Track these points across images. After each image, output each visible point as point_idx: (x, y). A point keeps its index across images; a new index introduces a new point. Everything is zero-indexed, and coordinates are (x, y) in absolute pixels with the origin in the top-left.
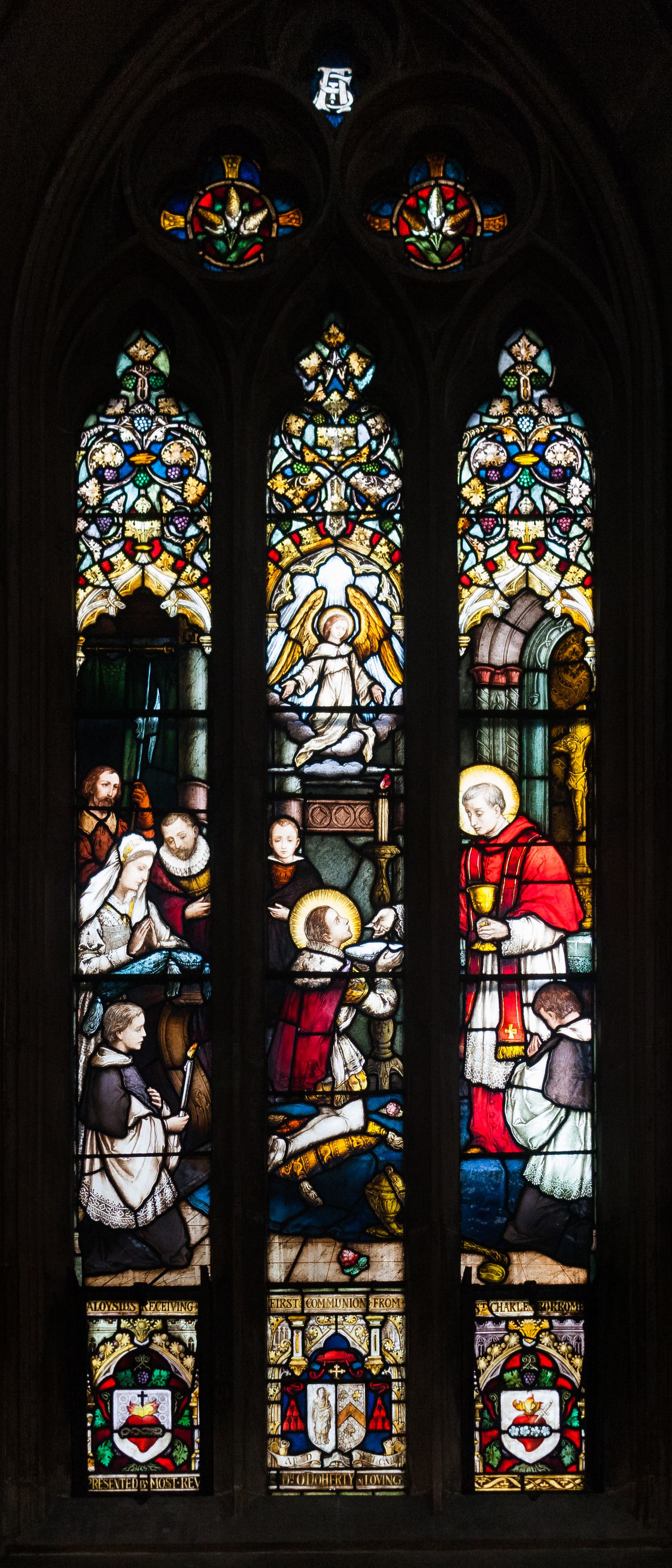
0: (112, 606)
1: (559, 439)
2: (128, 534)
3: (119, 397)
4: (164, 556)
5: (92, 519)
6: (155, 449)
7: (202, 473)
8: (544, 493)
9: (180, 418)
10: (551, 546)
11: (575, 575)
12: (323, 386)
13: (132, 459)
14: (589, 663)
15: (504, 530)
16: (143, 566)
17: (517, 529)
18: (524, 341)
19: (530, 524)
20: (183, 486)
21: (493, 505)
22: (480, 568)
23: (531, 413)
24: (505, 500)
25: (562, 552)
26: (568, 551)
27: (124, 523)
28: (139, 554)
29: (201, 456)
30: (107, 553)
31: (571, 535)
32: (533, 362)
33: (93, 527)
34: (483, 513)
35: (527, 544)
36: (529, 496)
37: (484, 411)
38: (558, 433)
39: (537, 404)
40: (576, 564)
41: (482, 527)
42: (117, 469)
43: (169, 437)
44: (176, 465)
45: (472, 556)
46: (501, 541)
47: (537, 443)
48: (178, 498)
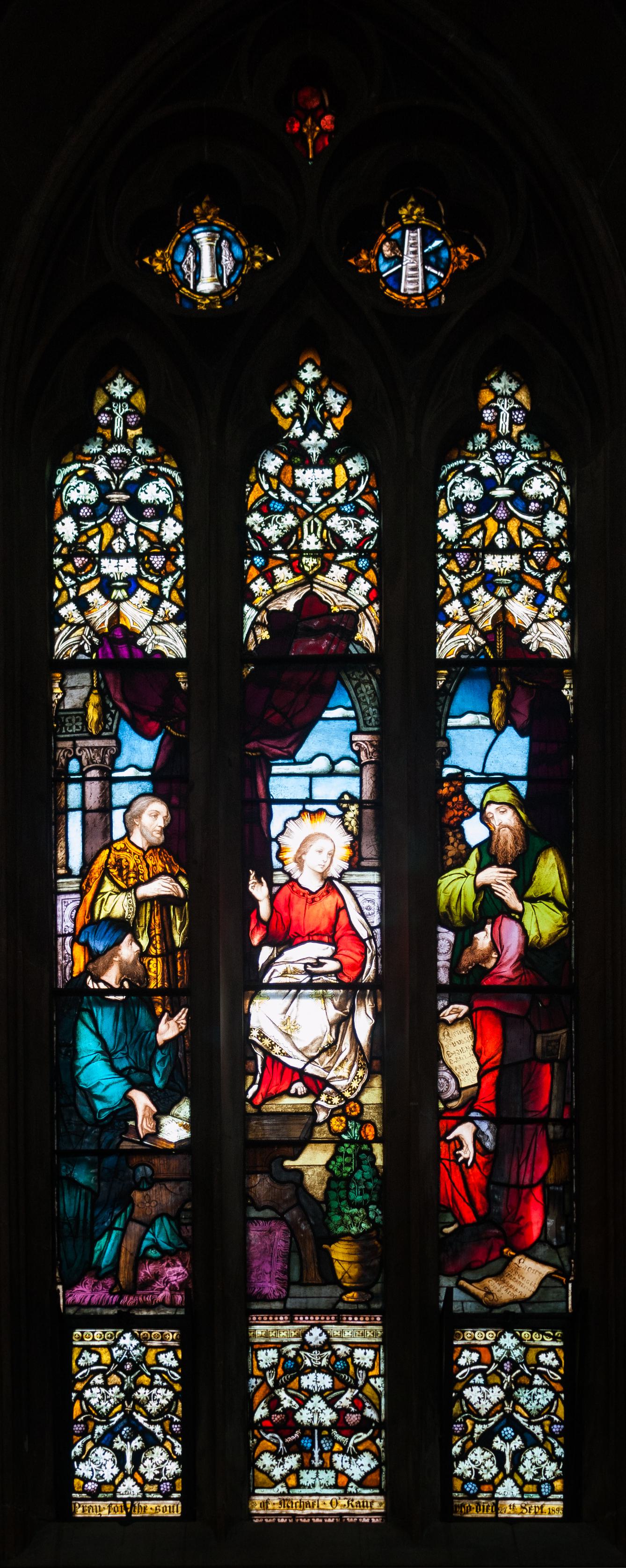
0: (469, 638)
1: (536, 474)
4: (140, 592)
5: (450, 554)
11: (169, 608)
12: (301, 423)
15: (480, 563)
16: (118, 602)
18: (120, 381)
19: (507, 558)
20: (542, 520)
23: (510, 450)
25: (154, 589)
27: (484, 557)
31: (549, 567)
32: (128, 399)
34: (77, 548)
35: (504, 577)
38: (536, 469)
40: (553, 596)
42: (93, 507)
45: (65, 593)
47: (514, 477)
48: (537, 533)
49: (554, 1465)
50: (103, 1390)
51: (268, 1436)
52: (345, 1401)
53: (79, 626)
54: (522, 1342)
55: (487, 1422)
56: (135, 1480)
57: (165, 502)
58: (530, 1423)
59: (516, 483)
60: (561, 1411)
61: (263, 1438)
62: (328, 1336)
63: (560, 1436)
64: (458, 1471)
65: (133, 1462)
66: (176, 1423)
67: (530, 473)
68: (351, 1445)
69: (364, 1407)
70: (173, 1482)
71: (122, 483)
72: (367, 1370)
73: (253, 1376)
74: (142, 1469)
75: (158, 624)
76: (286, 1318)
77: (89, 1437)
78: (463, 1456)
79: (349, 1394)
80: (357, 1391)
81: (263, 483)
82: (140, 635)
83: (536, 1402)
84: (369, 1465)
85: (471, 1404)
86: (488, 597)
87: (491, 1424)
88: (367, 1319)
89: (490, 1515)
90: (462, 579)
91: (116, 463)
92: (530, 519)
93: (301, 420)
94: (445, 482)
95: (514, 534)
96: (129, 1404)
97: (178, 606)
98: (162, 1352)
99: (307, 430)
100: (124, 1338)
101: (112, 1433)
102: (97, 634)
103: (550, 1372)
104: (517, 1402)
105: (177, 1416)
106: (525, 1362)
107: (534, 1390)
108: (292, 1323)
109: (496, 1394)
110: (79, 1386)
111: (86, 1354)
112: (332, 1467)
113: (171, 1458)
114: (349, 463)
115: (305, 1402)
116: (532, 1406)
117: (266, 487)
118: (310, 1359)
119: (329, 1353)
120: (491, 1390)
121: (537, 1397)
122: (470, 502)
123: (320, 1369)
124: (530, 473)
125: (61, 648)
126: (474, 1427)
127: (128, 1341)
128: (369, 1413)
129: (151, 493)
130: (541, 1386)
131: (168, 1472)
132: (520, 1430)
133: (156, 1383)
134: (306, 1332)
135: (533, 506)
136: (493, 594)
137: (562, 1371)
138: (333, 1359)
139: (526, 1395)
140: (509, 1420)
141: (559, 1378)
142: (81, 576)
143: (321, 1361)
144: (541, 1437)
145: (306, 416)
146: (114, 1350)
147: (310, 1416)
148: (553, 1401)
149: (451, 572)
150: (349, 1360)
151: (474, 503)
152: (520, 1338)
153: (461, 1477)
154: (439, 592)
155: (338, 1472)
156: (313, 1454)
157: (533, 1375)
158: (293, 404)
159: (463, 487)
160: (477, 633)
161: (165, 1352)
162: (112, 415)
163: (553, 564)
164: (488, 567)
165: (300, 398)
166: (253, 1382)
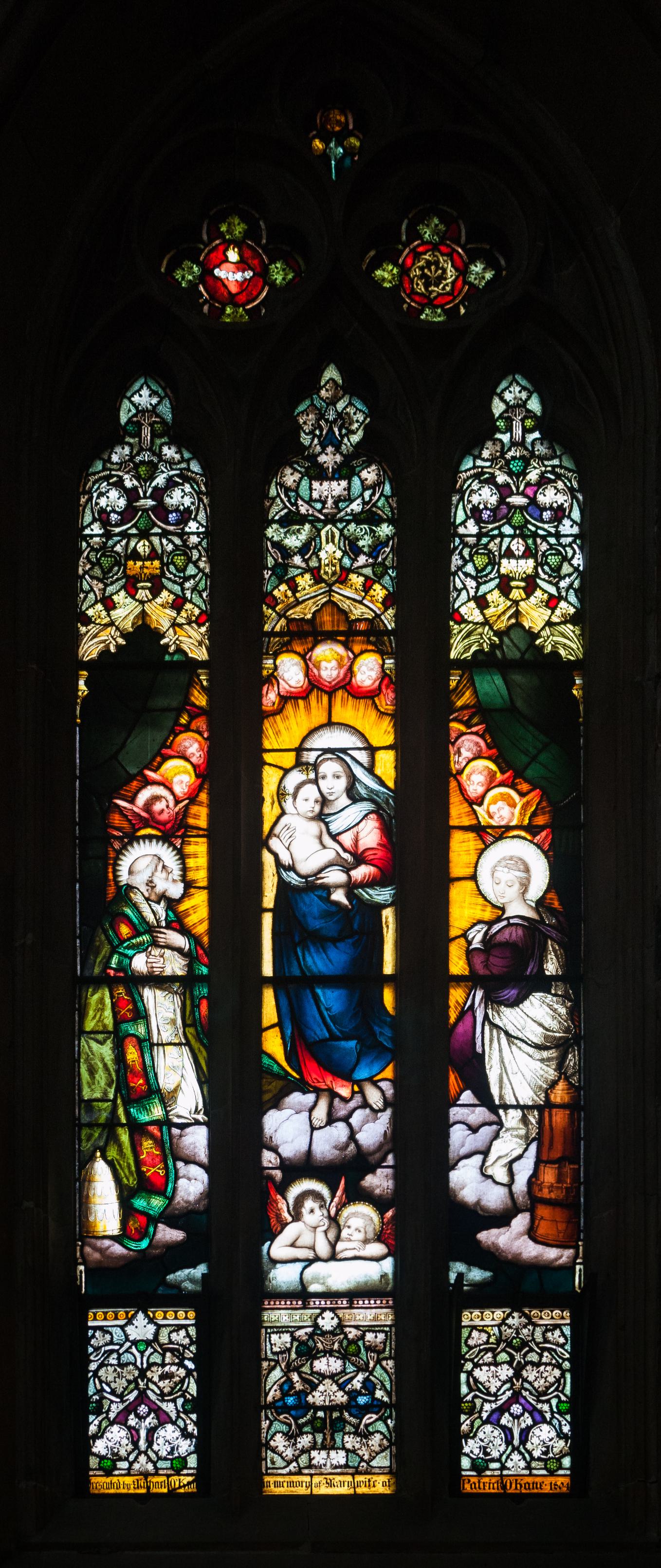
1: (177, 484)
3: (123, 443)
4: (165, 594)
6: (529, 492)
9: (183, 465)
13: (508, 500)
22: (472, 604)
26: (183, 589)
37: (476, 453)
38: (549, 475)
39: (530, 448)
41: (474, 565)
44: (551, 508)
45: (464, 593)
46: (118, 580)
47: (156, 488)
52: (357, 1384)
57: (562, 504)
59: (158, 494)
62: (339, 1319)
63: (566, 1413)
66: (564, 1402)
68: (362, 1427)
69: (375, 1388)
70: (559, 1460)
71: (150, 490)
72: (379, 1353)
77: (104, 1415)
79: (360, 1377)
80: (367, 1374)
83: (543, 1380)
86: (129, 600)
88: (378, 1302)
92: (171, 528)
96: (518, 1381)
97: (574, 607)
102: (123, 636)
105: (565, 1395)
106: (534, 1339)
108: (305, 1307)
109: (506, 1372)
111: (475, 1334)
114: (364, 474)
115: (318, 1385)
116: (540, 1384)
118: (322, 1343)
119: (342, 1336)
122: (114, 511)
123: (330, 1353)
124: (171, 484)
125: (86, 647)
126: (482, 1405)
127: (515, 1320)
128: (379, 1394)
129: (177, 498)
130: (550, 1364)
131: (555, 1449)
133: (544, 1360)
134: (318, 1316)
135: (172, 517)
136: (133, 597)
138: (345, 1343)
139: (535, 1372)
142: (107, 579)
147: (322, 1398)
149: (467, 575)
150: (360, 1343)
152: (528, 1317)
154: (82, 596)
155: (348, 1451)
157: (542, 1352)
159: (480, 495)
160: (118, 634)
161: (177, 1331)
164: (503, 571)
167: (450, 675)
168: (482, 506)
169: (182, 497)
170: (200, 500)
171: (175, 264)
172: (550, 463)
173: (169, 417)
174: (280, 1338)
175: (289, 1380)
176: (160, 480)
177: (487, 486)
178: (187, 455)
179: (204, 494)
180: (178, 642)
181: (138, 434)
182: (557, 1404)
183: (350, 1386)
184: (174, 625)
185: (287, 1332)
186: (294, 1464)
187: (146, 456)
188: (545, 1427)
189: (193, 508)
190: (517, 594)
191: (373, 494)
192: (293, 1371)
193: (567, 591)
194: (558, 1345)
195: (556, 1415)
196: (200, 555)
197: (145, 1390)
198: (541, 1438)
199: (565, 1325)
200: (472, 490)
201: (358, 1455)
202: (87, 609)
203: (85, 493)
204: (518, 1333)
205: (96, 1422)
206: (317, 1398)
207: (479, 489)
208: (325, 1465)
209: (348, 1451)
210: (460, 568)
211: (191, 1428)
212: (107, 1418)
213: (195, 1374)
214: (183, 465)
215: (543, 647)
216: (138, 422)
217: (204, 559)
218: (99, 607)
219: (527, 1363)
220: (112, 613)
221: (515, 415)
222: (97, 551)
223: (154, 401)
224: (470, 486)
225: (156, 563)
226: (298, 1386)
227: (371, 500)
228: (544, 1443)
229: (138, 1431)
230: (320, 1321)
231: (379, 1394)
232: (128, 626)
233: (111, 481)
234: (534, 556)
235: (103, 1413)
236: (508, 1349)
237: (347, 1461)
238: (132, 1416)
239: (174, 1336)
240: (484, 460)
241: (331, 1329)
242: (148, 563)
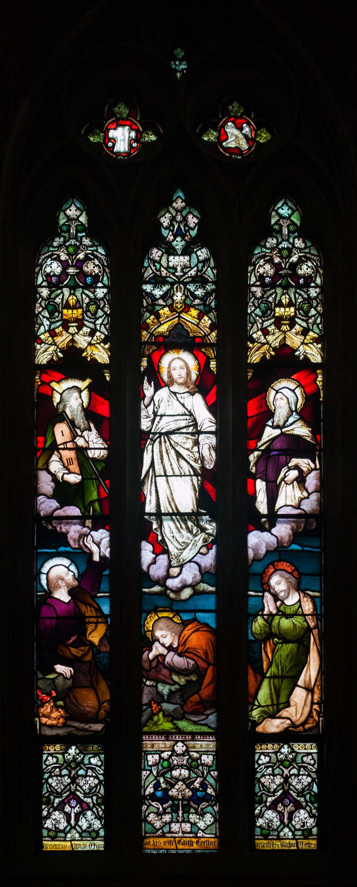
2: (277, 315)
3: (60, 237)
4: (297, 327)
7: (318, 281)
8: (83, 292)
9: (307, 251)
10: (86, 323)
12: (172, 233)
14: (319, 384)
17: (279, 311)
21: (55, 299)
24: (61, 297)
26: (95, 325)
28: (71, 328)
29: (104, 270)
30: (53, 326)
33: (258, 310)
36: (287, 293)
38: (90, 256)
41: (260, 309)
43: (300, 261)
47: (292, 264)
49: (312, 820)
50: (272, 777)
51: (153, 804)
52: (197, 785)
53: (264, 344)
54: (293, 751)
55: (274, 796)
56: (76, 830)
58: (85, 797)
60: (102, 791)
61: (151, 805)
64: (46, 826)
65: (288, 819)
67: (301, 261)
68: (199, 809)
69: (207, 788)
73: (144, 770)
74: (80, 823)
75: (306, 344)
76: (190, 737)
77: (263, 804)
78: (48, 816)
79: (199, 780)
81: (152, 266)
82: (297, 350)
83: (301, 784)
84: (210, 821)
85: (52, 787)
87: (276, 797)
89: (295, 848)
90: (50, 322)
91: (285, 253)
93: (173, 231)
94: (41, 266)
95: (80, 297)
98: (305, 756)
99: (175, 236)
100: (284, 748)
101: (279, 800)
103: (97, 768)
104: (78, 784)
107: (88, 778)
109: (279, 780)
110: (46, 776)
112: (189, 822)
113: (96, 818)
115: (175, 785)
117: (153, 268)
118: (177, 761)
119: (187, 757)
120: (276, 777)
121: (302, 781)
123: (182, 766)
124: (301, 261)
126: (267, 799)
128: (209, 791)
132: (80, 802)
133: (301, 773)
137: (103, 768)
138: (190, 761)
140: (73, 796)
141: (314, 770)
143: (183, 761)
144: (91, 805)
145: (175, 229)
146: (279, 754)
148: (97, 784)
151: (270, 277)
153: (47, 829)
155: (192, 824)
156: (178, 814)
158: (168, 221)
159: (264, 268)
160: (58, 350)
161: (307, 756)
162: (281, 226)
163: (100, 313)
165: (173, 219)
166: (144, 773)
167: (248, 372)
168: (265, 275)
169: (94, 267)
170: (104, 270)
171: (204, 131)
172: (92, 249)
173: (298, 223)
174: (153, 757)
175: (158, 782)
176: (294, 259)
177: (55, 262)
178: (309, 244)
179: (319, 267)
180: (304, 354)
181: (68, 231)
182: (310, 798)
183: (192, 786)
184: (90, 344)
185: (157, 754)
186: (161, 831)
187: (285, 245)
188: (302, 811)
189: (313, 275)
190: (285, 328)
191: (203, 266)
192: (161, 776)
193: (313, 326)
194: (309, 764)
195: (309, 804)
196: (105, 304)
197: (288, 790)
198: (300, 818)
199: (314, 753)
200: (260, 265)
201: (197, 826)
202: (253, 334)
203: (38, 266)
204: (286, 757)
205: (259, 808)
206: (173, 792)
207: (51, 264)
208: (179, 832)
209: (192, 824)
210: (253, 312)
211: (314, 811)
212: (265, 806)
213: (316, 780)
214: (307, 251)
215: (299, 356)
216: (69, 225)
217: (107, 306)
218: (260, 333)
219: (291, 775)
220: (267, 337)
221: (72, 224)
222: (46, 300)
223: (78, 213)
224: (259, 262)
225: (292, 309)
226: (163, 786)
227: (202, 270)
228: (302, 821)
229: (283, 814)
230: (176, 748)
231: (209, 791)
232: (276, 344)
233: (53, 258)
234: (294, 305)
235: (263, 803)
236: (281, 767)
237: (191, 830)
238: (280, 805)
239: (305, 759)
240: (267, 248)
241: (182, 752)
242: (287, 309)
